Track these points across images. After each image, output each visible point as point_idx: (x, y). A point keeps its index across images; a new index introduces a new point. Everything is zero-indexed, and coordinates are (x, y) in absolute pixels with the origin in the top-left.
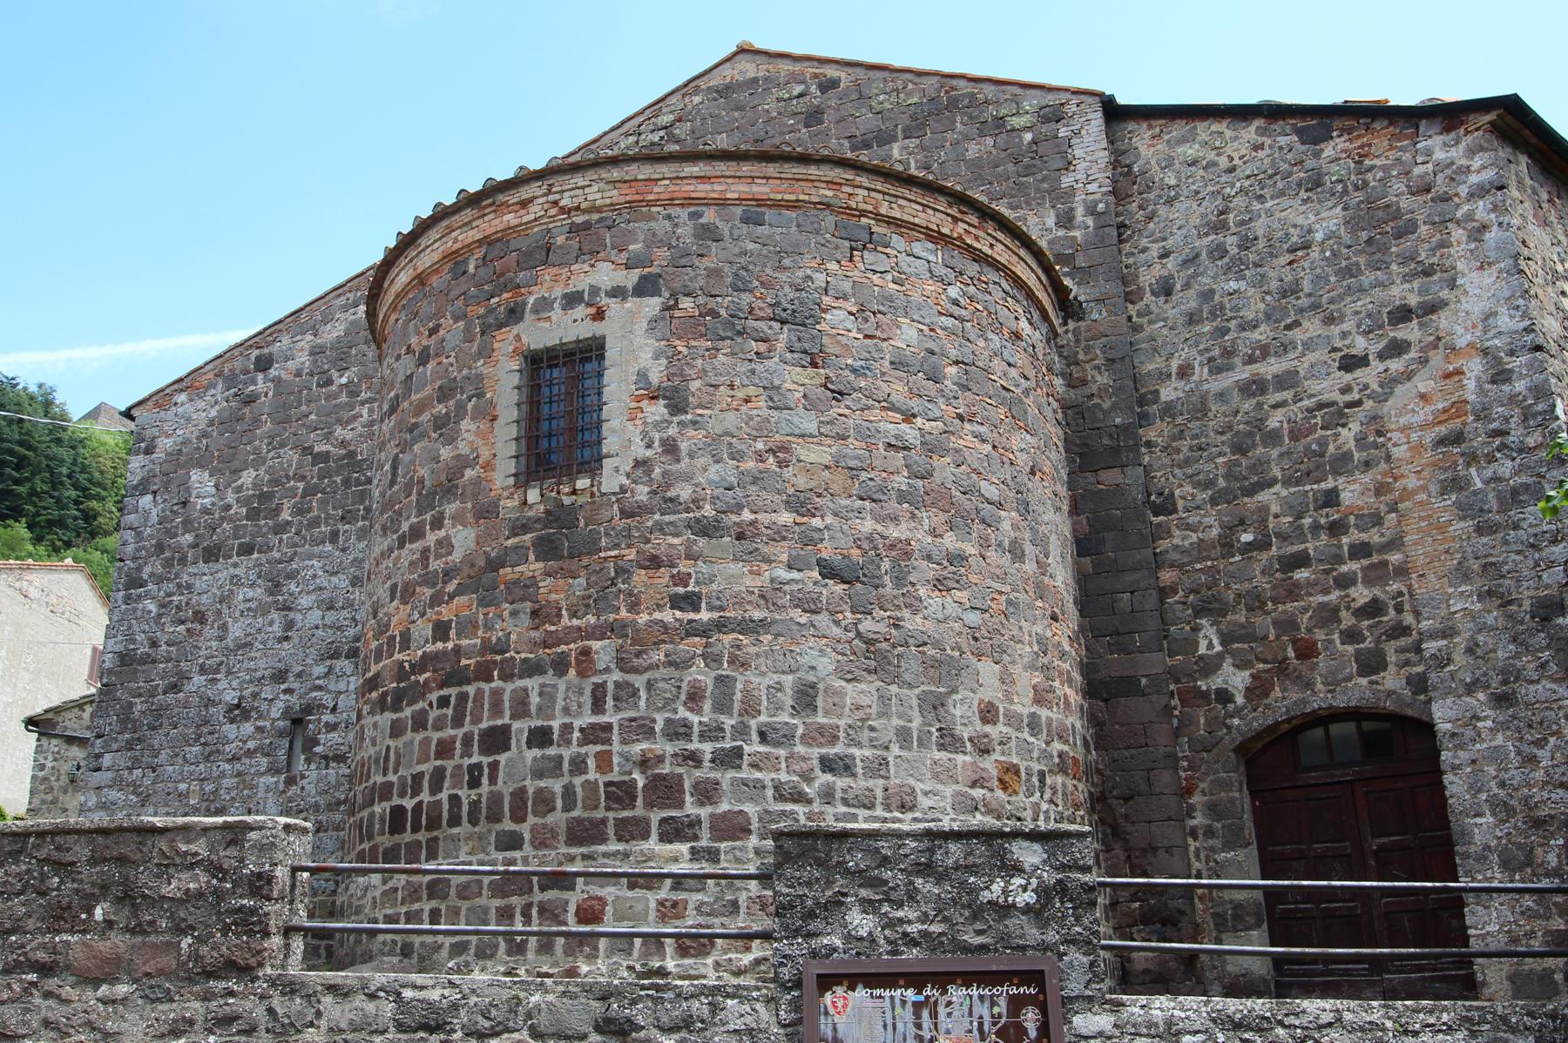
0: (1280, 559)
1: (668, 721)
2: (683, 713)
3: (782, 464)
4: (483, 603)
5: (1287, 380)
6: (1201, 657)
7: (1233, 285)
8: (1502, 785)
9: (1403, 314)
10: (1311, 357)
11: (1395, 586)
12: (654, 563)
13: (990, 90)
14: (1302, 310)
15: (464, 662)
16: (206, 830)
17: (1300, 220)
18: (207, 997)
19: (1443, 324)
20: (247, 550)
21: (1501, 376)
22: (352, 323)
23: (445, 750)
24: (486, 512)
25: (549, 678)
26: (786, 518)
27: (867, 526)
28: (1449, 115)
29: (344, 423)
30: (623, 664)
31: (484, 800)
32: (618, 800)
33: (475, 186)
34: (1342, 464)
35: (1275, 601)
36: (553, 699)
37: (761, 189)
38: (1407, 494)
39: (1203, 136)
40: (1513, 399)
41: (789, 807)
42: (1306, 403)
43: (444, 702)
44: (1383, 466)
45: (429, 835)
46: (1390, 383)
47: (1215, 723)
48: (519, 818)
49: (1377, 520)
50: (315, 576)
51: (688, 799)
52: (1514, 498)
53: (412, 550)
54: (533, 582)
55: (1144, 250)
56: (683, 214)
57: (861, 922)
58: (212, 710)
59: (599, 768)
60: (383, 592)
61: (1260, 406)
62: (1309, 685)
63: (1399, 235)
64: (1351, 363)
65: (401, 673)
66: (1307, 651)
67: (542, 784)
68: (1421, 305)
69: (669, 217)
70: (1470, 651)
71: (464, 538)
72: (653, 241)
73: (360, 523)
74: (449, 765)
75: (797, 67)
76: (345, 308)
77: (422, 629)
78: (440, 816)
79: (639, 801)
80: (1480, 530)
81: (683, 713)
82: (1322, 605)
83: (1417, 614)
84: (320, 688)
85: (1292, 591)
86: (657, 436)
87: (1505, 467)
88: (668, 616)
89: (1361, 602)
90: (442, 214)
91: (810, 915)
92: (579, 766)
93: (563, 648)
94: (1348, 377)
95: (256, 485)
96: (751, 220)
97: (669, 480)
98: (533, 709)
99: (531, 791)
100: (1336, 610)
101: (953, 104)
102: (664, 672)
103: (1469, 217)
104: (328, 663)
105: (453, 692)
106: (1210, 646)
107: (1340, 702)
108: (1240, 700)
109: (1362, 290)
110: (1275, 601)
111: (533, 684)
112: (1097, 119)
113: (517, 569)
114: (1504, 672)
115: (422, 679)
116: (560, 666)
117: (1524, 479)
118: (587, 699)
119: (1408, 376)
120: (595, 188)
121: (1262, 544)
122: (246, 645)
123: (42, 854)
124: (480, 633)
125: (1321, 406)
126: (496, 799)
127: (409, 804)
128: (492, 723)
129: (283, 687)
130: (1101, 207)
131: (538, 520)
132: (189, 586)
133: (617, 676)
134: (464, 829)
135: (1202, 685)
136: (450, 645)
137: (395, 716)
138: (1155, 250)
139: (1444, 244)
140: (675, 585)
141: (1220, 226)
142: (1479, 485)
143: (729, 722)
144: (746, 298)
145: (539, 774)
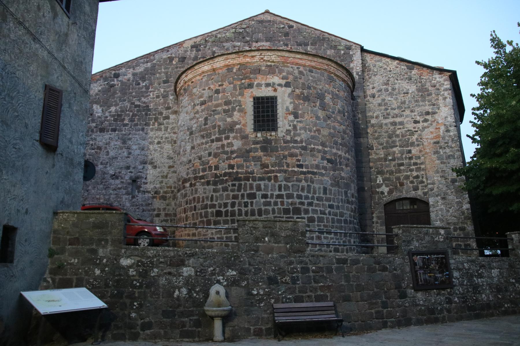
1: (297, 194)
4: (244, 161)
5: (401, 123)
6: (378, 184)
7: (390, 99)
8: (442, 216)
9: (428, 113)
12: (292, 155)
14: (405, 108)
15: (240, 175)
17: (406, 87)
20: (114, 130)
21: (448, 131)
22: (146, 68)
25: (266, 182)
26: (320, 148)
27: (334, 151)
28: (441, 71)
29: (145, 97)
34: (412, 144)
37: (313, 64)
38: (426, 153)
40: (450, 136)
41: (323, 216)
42: (406, 129)
43: (234, 185)
44: (421, 146)
46: (424, 128)
47: (380, 198)
49: (419, 158)
51: (302, 213)
55: (368, 86)
56: (295, 67)
58: (106, 176)
59: (281, 205)
61: (395, 128)
62: (402, 192)
63: (428, 95)
64: (416, 122)
66: (402, 184)
67: (267, 207)
68: (432, 112)
70: (437, 188)
72: (289, 73)
73: (151, 127)
75: (282, 20)
76: (143, 63)
79: (291, 213)
81: (300, 193)
82: (406, 175)
83: (427, 179)
84: (141, 172)
85: (400, 171)
86: (292, 124)
88: (296, 169)
89: (415, 175)
93: (269, 175)
94: (415, 125)
95: (116, 111)
96: (311, 71)
100: (409, 176)
101: (324, 39)
103: (443, 95)
104: (143, 165)
105: (237, 183)
106: (380, 181)
108: (386, 194)
109: (419, 106)
110: (396, 173)
111: (262, 183)
112: (359, 51)
115: (225, 178)
116: (269, 179)
117: (451, 153)
120: (274, 56)
121: (393, 160)
122: (115, 158)
123: (250, 225)
125: (409, 131)
127: (223, 210)
128: (250, 192)
129: (129, 171)
130: (360, 73)
131: (261, 141)
132: (95, 139)
135: (378, 190)
136: (235, 171)
137: (214, 187)
138: (371, 86)
141: (387, 84)
142: (442, 153)
143: (310, 196)
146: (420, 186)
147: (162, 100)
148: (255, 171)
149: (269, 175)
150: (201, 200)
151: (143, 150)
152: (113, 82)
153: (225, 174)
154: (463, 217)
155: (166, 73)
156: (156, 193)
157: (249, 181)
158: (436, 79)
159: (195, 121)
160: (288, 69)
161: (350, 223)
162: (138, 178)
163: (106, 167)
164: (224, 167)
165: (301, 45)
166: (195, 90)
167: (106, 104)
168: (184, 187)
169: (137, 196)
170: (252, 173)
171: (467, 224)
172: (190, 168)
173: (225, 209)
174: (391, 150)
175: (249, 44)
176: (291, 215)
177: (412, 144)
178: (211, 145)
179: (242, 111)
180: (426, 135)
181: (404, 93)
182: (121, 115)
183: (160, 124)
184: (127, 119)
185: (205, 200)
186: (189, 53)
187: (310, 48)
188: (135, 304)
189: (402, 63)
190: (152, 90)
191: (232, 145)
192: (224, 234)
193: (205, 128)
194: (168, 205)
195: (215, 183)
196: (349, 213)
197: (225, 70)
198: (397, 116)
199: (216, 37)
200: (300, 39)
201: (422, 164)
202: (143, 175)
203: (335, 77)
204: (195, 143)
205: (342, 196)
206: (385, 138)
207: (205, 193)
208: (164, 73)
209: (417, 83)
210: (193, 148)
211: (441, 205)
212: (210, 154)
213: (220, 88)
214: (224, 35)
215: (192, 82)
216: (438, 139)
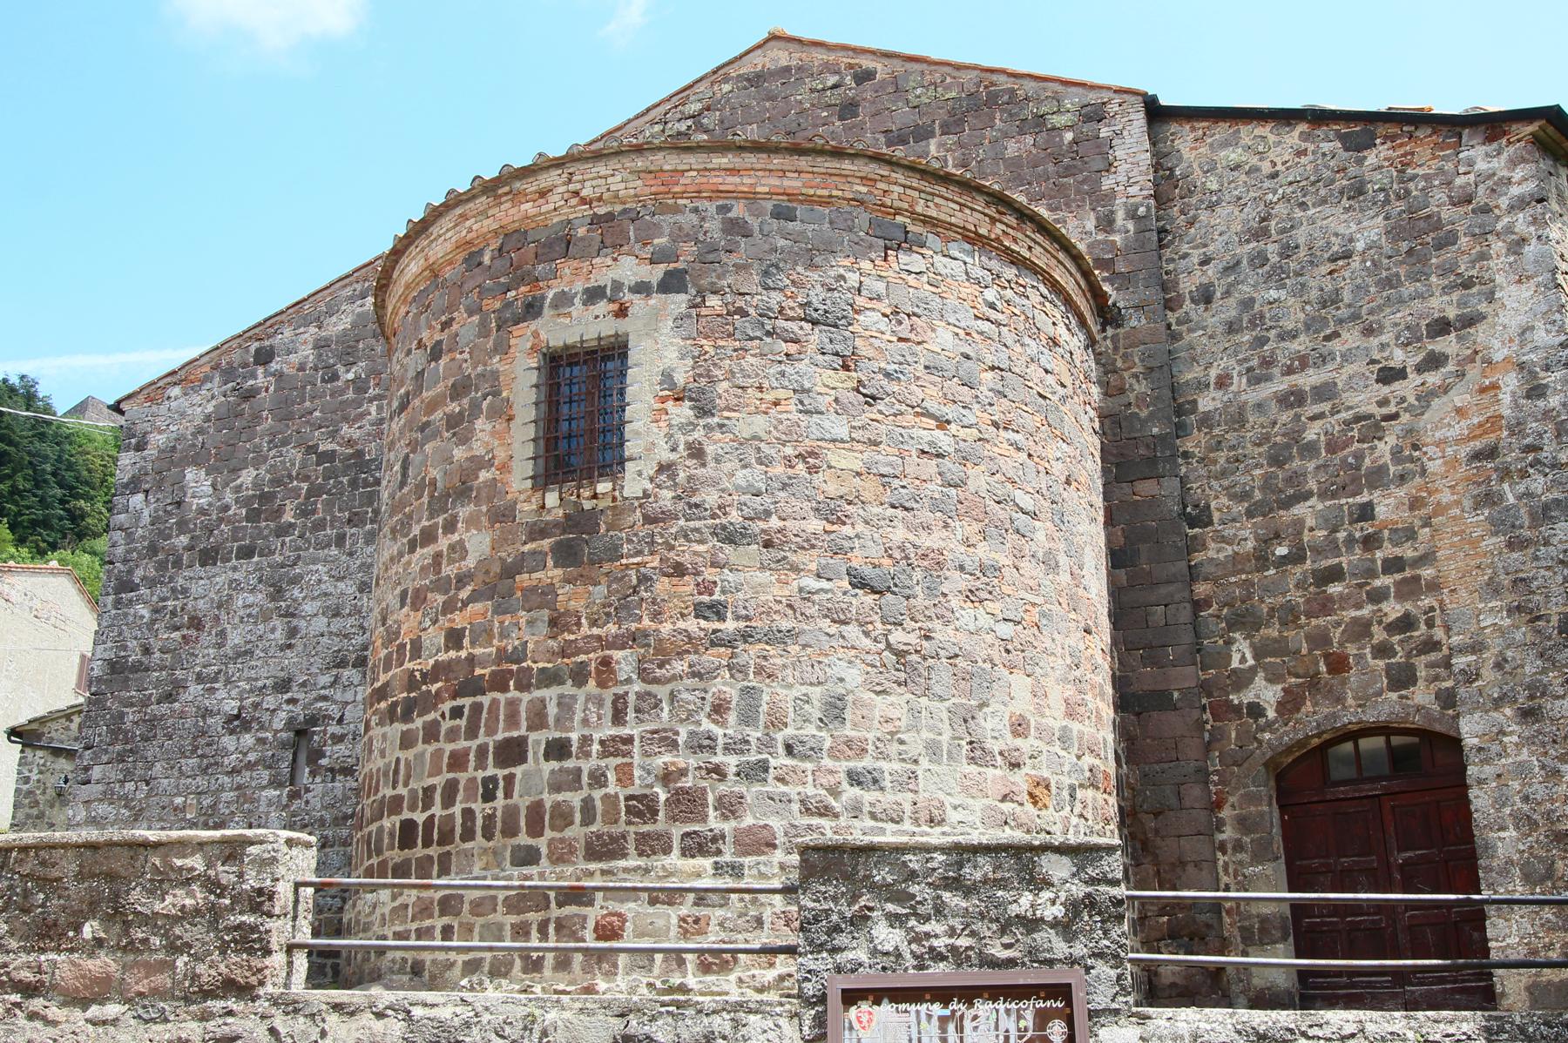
0: (1314, 572)
1: (692, 734)
2: (707, 725)
4: (498, 610)
5: (1325, 392)
6: (1234, 671)
7: (1273, 294)
8: (1526, 799)
9: (1441, 327)
10: (1349, 369)
12: (679, 570)
13: (1030, 86)
14: (1341, 321)
15: (478, 671)
16: (201, 845)
17: (1341, 229)
20: (246, 553)
21: (1536, 391)
22: (359, 315)
23: (458, 761)
25: (568, 688)
26: (815, 525)
27: (899, 534)
28: (1492, 125)
30: (644, 675)
31: (499, 813)
32: (639, 814)
33: (490, 173)
34: (1377, 478)
35: (1308, 617)
37: (792, 183)
38: (1440, 509)
39: (1246, 140)
40: (1547, 414)
41: (815, 821)
42: (1344, 415)
43: (457, 713)
44: (1418, 479)
46: (1426, 397)
47: (1247, 737)
48: (535, 829)
49: (1410, 534)
53: (424, 554)
56: (711, 207)
57: (887, 936)
58: (210, 721)
60: (392, 599)
61: (1297, 417)
62: (1340, 700)
63: (1439, 246)
64: (1389, 375)
65: (411, 683)
66: (1338, 665)
67: (560, 797)
68: (1460, 318)
69: (696, 210)
70: (1498, 666)
72: (679, 235)
73: (368, 527)
74: (463, 777)
76: (351, 300)
77: (434, 637)
78: (452, 830)
80: (1511, 545)
81: (707, 725)
82: (1355, 620)
83: (1448, 629)
84: (325, 698)
85: (1325, 606)
86: (682, 440)
88: (692, 625)
89: (1393, 617)
90: (455, 200)
92: (598, 779)
93: (583, 657)
94: (1386, 390)
95: (257, 484)
98: (551, 720)
99: (548, 805)
100: (1368, 624)
101: (992, 99)
103: (1509, 230)
104: (334, 672)
105: (467, 702)
106: (1243, 660)
108: (1271, 714)
109: (1401, 301)
110: (1308, 617)
111: (550, 694)
112: (1139, 119)
113: (535, 575)
115: (434, 688)
116: (579, 676)
117: (1556, 495)
118: (608, 710)
119: (1445, 389)
121: (1297, 557)
122: (246, 653)
123: (25, 870)
124: (495, 642)
125: (1358, 419)
126: (511, 814)
127: (420, 818)
128: (507, 735)
131: (556, 525)
132: (185, 591)
133: (638, 687)
135: (1234, 698)
136: (463, 654)
137: (405, 727)
140: (700, 593)
141: (1260, 233)
142: (1512, 500)
144: (776, 297)
145: (556, 788)
146: (1420, 662)
148: (530, 646)
149: (583, 657)
151: (337, 614)
152: (251, 382)
157: (505, 689)
160: (679, 217)
162: (313, 720)
163: (212, 690)
165: (904, 142)
167: (224, 464)
170: (518, 656)
174: (1285, 516)
181: (1333, 260)
182: (272, 496)
184: (290, 506)
187: (941, 145)
189: (1321, 132)
198: (1303, 362)
200: (902, 116)
202: (334, 710)
206: (1257, 466)
209: (1387, 201)
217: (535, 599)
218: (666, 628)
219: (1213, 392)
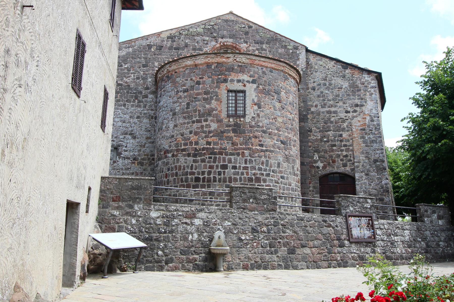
0: (331, 144)
1: (258, 167)
2: (261, 166)
3: (276, 121)
4: (219, 139)
5: (335, 112)
7: (327, 92)
8: (365, 188)
9: (357, 105)
10: (340, 109)
11: (350, 153)
12: (256, 137)
13: (284, 38)
14: (339, 100)
15: (215, 151)
16: (266, 189)
17: (341, 83)
18: (270, 214)
19: (364, 109)
21: (372, 121)
22: (128, 52)
24: (219, 121)
25: (236, 156)
26: (276, 132)
27: (286, 134)
28: (369, 72)
29: (127, 78)
30: (250, 155)
32: (250, 181)
34: (343, 130)
35: (329, 152)
36: (237, 160)
37: (273, 66)
38: (355, 137)
39: (324, 61)
40: (374, 125)
41: (276, 184)
43: (210, 158)
44: (351, 132)
45: (207, 183)
46: (354, 117)
49: (349, 141)
50: (119, 114)
52: (372, 142)
54: (232, 137)
55: (310, 80)
56: (260, 68)
57: (351, 209)
61: (330, 116)
62: (334, 167)
64: (347, 112)
68: (360, 105)
69: (257, 68)
71: (214, 126)
72: (255, 72)
73: (132, 103)
74: (213, 171)
76: (126, 48)
78: (211, 180)
80: (366, 146)
81: (261, 166)
83: (354, 158)
84: (122, 141)
85: (333, 151)
87: (371, 136)
91: (346, 207)
92: (242, 174)
94: (346, 114)
97: (258, 121)
99: (233, 177)
100: (340, 155)
101: (276, 39)
102: (257, 158)
103: (370, 91)
105: (213, 156)
106: (316, 158)
107: (339, 171)
108: (321, 168)
110: (329, 152)
111: (232, 157)
114: (368, 170)
115: (203, 152)
116: (238, 154)
117: (374, 139)
118: (244, 162)
119: (356, 117)
121: (328, 141)
123: (240, 191)
125: (341, 118)
127: (201, 177)
130: (304, 70)
133: (249, 158)
134: (217, 183)
136: (211, 147)
137: (194, 159)
138: (312, 81)
139: (365, 95)
143: (268, 168)
144: (270, 88)
145: (234, 174)
147: (142, 81)
148: (228, 147)
150: (182, 168)
153: (204, 149)
154: (382, 190)
155: (146, 58)
156: (135, 159)
157: (222, 155)
158: (365, 77)
159: (178, 104)
161: (296, 191)
164: (202, 143)
165: (258, 43)
166: (178, 79)
168: (166, 157)
169: (118, 162)
170: (225, 149)
171: (385, 196)
172: (173, 142)
173: (203, 176)
175: (216, 39)
176: (254, 183)
177: (343, 130)
178: (193, 125)
179: (219, 100)
180: (355, 123)
183: (140, 102)
185: (186, 168)
186: (165, 42)
188: (161, 244)
189: (338, 63)
190: (133, 72)
191: (210, 127)
192: (201, 196)
193: (187, 111)
194: (144, 170)
195: (195, 156)
196: (295, 183)
197: (205, 67)
198: (332, 106)
199: (188, 31)
201: (350, 146)
203: (288, 76)
204: (178, 122)
205: (290, 169)
207: (186, 163)
208: (144, 58)
210: (176, 126)
211: (364, 180)
212: (191, 132)
213: (201, 80)
214: (195, 30)
215: (175, 73)
216: (364, 127)
217: (228, 139)
218: (254, 148)
219: (314, 108)
